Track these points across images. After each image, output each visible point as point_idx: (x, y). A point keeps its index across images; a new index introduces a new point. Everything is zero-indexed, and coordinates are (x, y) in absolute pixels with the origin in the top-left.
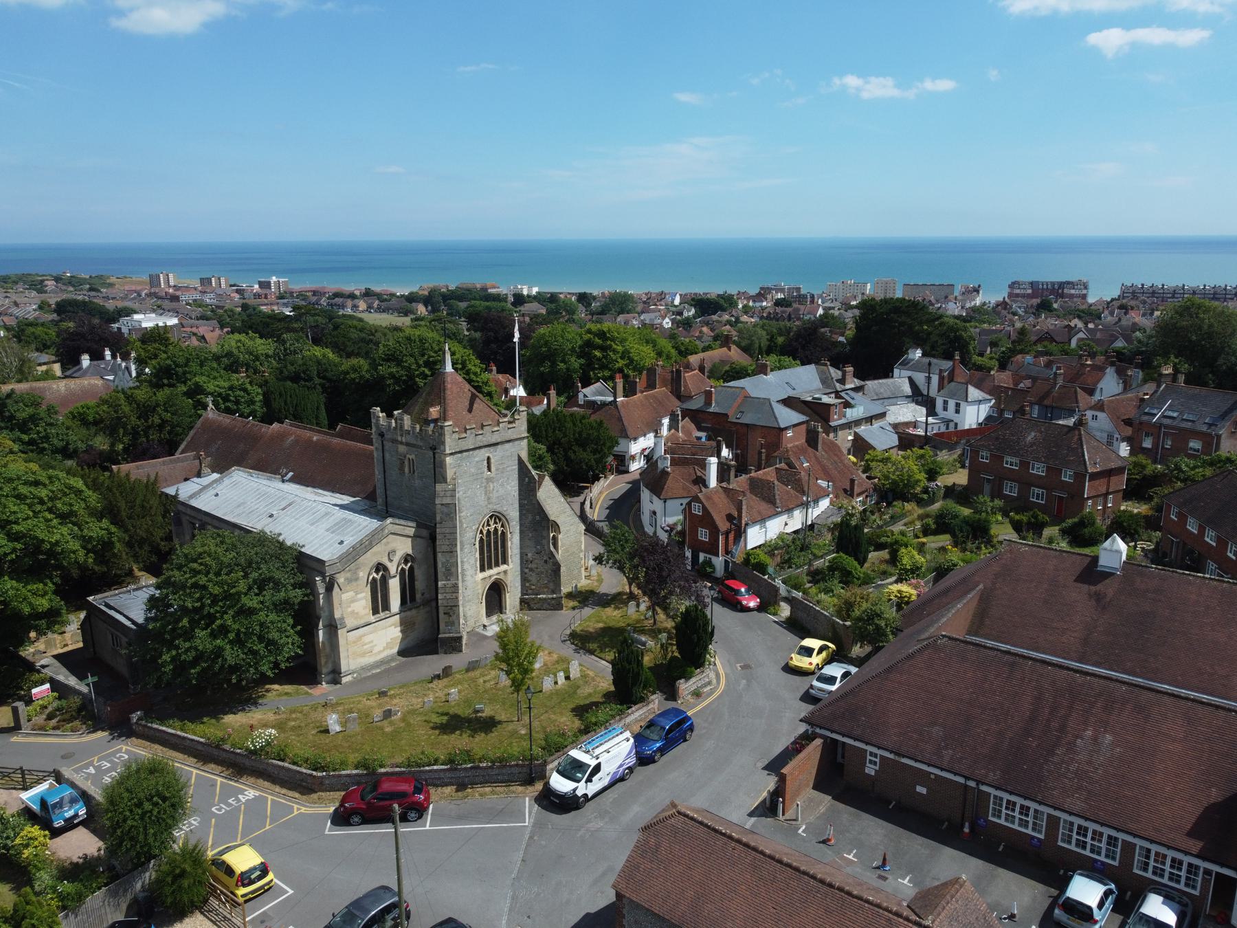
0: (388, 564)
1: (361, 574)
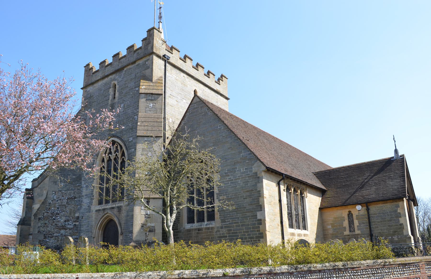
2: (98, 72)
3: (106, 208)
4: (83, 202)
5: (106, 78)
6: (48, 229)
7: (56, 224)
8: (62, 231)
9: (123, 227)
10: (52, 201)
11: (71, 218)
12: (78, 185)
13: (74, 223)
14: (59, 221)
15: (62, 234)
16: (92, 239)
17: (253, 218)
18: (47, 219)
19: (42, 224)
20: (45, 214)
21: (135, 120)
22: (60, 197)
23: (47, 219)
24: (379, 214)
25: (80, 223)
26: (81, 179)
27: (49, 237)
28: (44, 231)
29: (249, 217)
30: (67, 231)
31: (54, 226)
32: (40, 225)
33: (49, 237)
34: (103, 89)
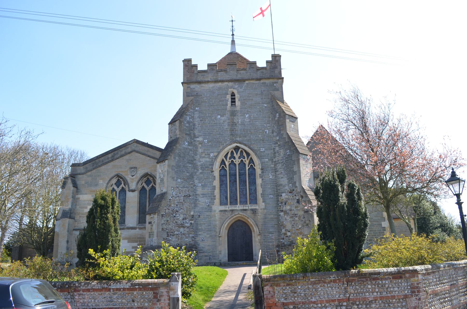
0: (129, 178)
1: (101, 182)
2: (206, 73)
3: (235, 210)
4: (199, 201)
5: (220, 83)
6: (170, 226)
7: (176, 222)
8: (182, 230)
9: (260, 228)
10: (172, 197)
11: (188, 216)
12: (191, 183)
13: (190, 222)
14: (178, 219)
15: (181, 232)
16: (218, 238)
17: (379, 226)
18: (168, 216)
19: (165, 221)
20: (167, 211)
21: (266, 133)
22: (178, 194)
23: (168, 216)
24: (399, 227)
25: (195, 221)
26: (193, 177)
27: (171, 235)
28: (167, 229)
29: (375, 225)
30: (185, 229)
31: (175, 224)
32: (163, 222)
33: (171, 235)
34: (217, 92)
